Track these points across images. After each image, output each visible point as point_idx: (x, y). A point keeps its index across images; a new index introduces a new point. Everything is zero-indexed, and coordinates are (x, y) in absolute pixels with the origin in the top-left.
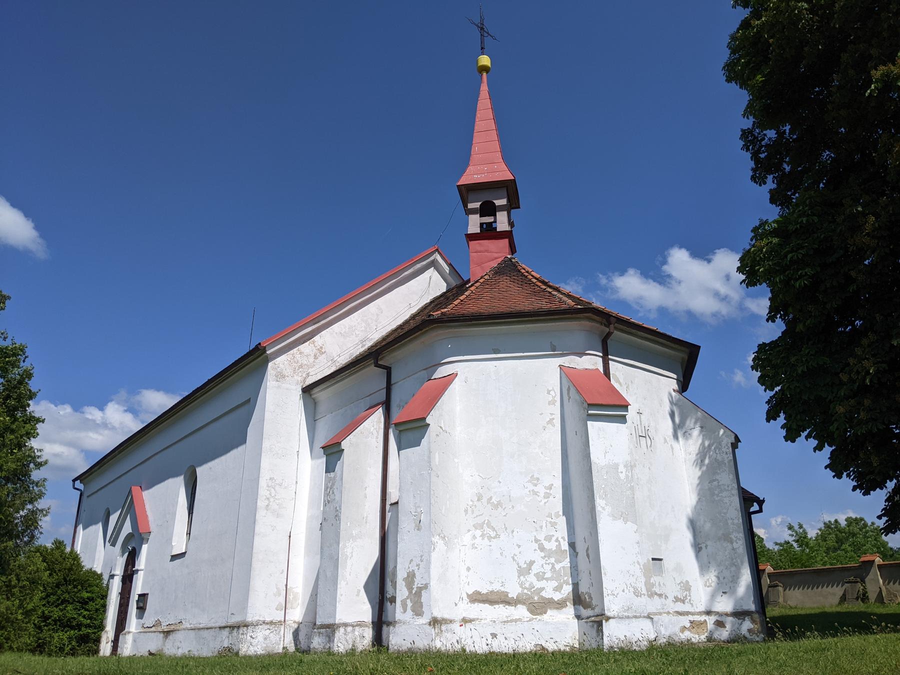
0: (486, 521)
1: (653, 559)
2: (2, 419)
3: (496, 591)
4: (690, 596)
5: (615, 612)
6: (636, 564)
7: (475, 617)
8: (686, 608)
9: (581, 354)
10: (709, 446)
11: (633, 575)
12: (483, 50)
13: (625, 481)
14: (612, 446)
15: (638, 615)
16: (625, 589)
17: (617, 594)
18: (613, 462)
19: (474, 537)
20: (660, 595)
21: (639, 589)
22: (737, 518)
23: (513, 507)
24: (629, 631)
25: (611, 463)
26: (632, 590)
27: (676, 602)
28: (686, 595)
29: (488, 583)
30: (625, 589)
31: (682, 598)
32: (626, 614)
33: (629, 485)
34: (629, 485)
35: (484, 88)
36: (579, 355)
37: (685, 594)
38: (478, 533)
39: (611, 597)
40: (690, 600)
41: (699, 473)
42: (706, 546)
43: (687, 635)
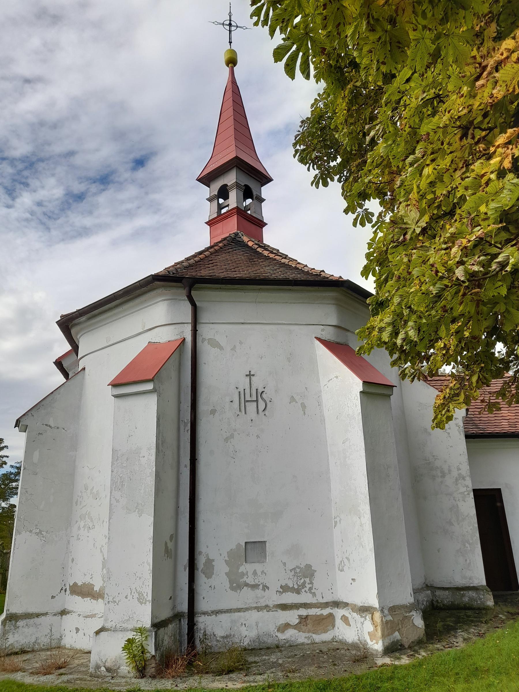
2: (518, 391)
3: (87, 583)
4: (311, 583)
5: (113, 623)
6: (146, 564)
8: (305, 598)
11: (140, 578)
14: (136, 428)
20: (254, 587)
21: (145, 595)
26: (136, 595)
27: (283, 592)
28: (305, 582)
29: (83, 575)
31: (296, 587)
32: (125, 625)
37: (302, 581)
40: (310, 589)
43: (290, 634)
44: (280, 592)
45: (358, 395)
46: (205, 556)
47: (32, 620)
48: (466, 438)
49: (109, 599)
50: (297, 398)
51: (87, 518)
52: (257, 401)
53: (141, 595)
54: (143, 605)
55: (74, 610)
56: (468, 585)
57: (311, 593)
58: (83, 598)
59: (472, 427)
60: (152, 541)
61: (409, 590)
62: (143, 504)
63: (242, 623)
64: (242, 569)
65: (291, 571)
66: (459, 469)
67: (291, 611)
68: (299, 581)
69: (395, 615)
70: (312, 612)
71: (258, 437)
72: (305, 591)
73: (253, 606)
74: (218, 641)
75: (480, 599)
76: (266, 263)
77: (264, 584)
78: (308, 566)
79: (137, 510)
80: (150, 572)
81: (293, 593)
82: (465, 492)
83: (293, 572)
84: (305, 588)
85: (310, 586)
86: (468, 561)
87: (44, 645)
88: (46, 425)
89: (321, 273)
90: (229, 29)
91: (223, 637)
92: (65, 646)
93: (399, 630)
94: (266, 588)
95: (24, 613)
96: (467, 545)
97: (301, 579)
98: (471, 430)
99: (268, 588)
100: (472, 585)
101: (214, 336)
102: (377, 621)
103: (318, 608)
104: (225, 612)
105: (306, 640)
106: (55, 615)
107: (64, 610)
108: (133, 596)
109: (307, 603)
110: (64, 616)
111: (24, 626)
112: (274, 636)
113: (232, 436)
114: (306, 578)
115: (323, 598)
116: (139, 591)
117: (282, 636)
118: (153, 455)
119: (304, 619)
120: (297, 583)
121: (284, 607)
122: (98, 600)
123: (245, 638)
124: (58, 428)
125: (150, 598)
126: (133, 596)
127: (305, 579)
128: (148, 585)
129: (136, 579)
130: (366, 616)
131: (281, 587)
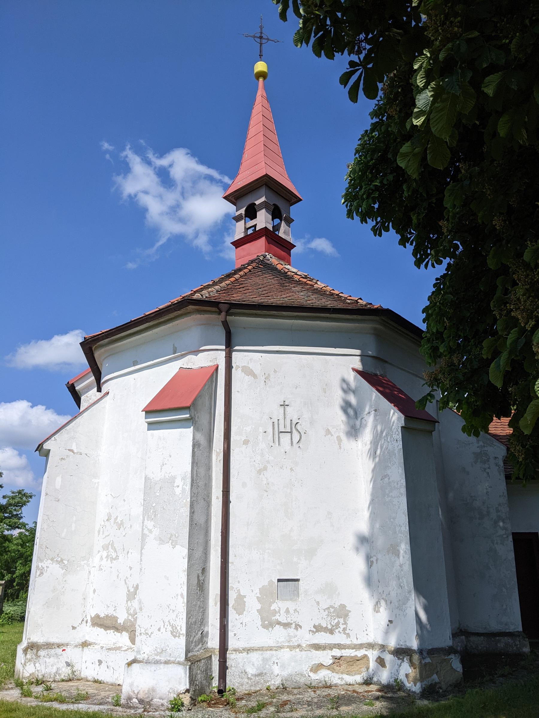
0: (111, 542)
1: (279, 580)
3: (110, 615)
4: (345, 623)
5: (145, 655)
6: (179, 596)
7: (94, 641)
8: (338, 638)
9: (196, 352)
10: (382, 432)
11: (174, 611)
12: (261, 57)
13: (180, 496)
14: (170, 457)
15: (172, 659)
16: (162, 627)
17: (152, 633)
18: (170, 475)
19: (102, 558)
20: (287, 625)
21: (178, 628)
22: (404, 525)
23: (131, 526)
24: (154, 679)
25: (167, 477)
26: (169, 628)
27: (317, 632)
28: (338, 623)
29: (106, 607)
30: (162, 627)
32: (158, 658)
33: (184, 501)
34: (184, 501)
35: (261, 92)
36: (195, 353)
37: (336, 621)
38: (105, 554)
39: (144, 637)
40: (344, 629)
41: (372, 466)
42: (377, 560)
43: (323, 675)
44: (313, 631)
45: (400, 430)
46: (236, 591)
47: (53, 650)
48: (506, 479)
49: (140, 630)
50: (333, 431)
51: (110, 549)
52: (291, 432)
53: (174, 628)
54: (176, 638)
55: (96, 642)
56: (504, 631)
57: (345, 633)
58: (106, 630)
59: (510, 467)
60: (186, 573)
61: (448, 633)
62: (177, 535)
63: (274, 662)
64: (274, 607)
65: (324, 610)
66: (498, 511)
67: (324, 651)
68: (333, 621)
69: (433, 657)
70: (347, 653)
71: (292, 469)
72: (339, 632)
73: (285, 645)
74: (248, 678)
75: (516, 645)
76: (298, 288)
77: (297, 623)
78: (343, 606)
79: (171, 541)
80: (184, 605)
81: (327, 633)
82: (503, 534)
83: (327, 611)
84: (339, 629)
85: (345, 626)
86: (504, 607)
87: (65, 676)
88: (69, 450)
89: (359, 301)
90: (259, 42)
91: (256, 676)
92: (87, 678)
93: (437, 673)
94: (298, 627)
95: (45, 643)
96: (504, 590)
97: (335, 619)
98: (509, 470)
99: (301, 627)
100: (507, 631)
101: (248, 363)
102: (416, 663)
103: (353, 649)
104: (256, 650)
105: (339, 680)
106: (76, 646)
107: (85, 642)
108: (166, 628)
109: (340, 644)
110: (85, 648)
111: (46, 656)
112: (307, 675)
113: (265, 469)
114: (340, 618)
115: (357, 639)
116: (172, 624)
117: (314, 677)
118: (188, 485)
119: (337, 659)
120: (330, 623)
121: (317, 647)
122: (123, 633)
123: (277, 676)
124: (81, 454)
125: (184, 631)
126: (166, 628)
127: (339, 619)
128: (182, 619)
129: (169, 612)
130: (404, 658)
131: (315, 626)
